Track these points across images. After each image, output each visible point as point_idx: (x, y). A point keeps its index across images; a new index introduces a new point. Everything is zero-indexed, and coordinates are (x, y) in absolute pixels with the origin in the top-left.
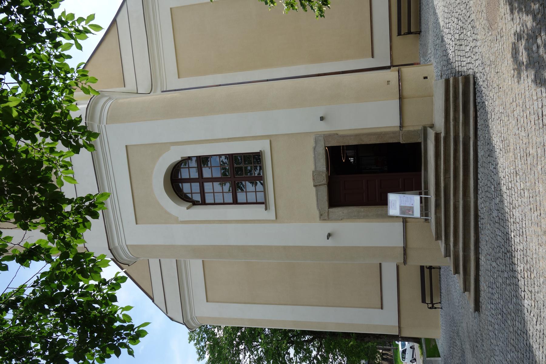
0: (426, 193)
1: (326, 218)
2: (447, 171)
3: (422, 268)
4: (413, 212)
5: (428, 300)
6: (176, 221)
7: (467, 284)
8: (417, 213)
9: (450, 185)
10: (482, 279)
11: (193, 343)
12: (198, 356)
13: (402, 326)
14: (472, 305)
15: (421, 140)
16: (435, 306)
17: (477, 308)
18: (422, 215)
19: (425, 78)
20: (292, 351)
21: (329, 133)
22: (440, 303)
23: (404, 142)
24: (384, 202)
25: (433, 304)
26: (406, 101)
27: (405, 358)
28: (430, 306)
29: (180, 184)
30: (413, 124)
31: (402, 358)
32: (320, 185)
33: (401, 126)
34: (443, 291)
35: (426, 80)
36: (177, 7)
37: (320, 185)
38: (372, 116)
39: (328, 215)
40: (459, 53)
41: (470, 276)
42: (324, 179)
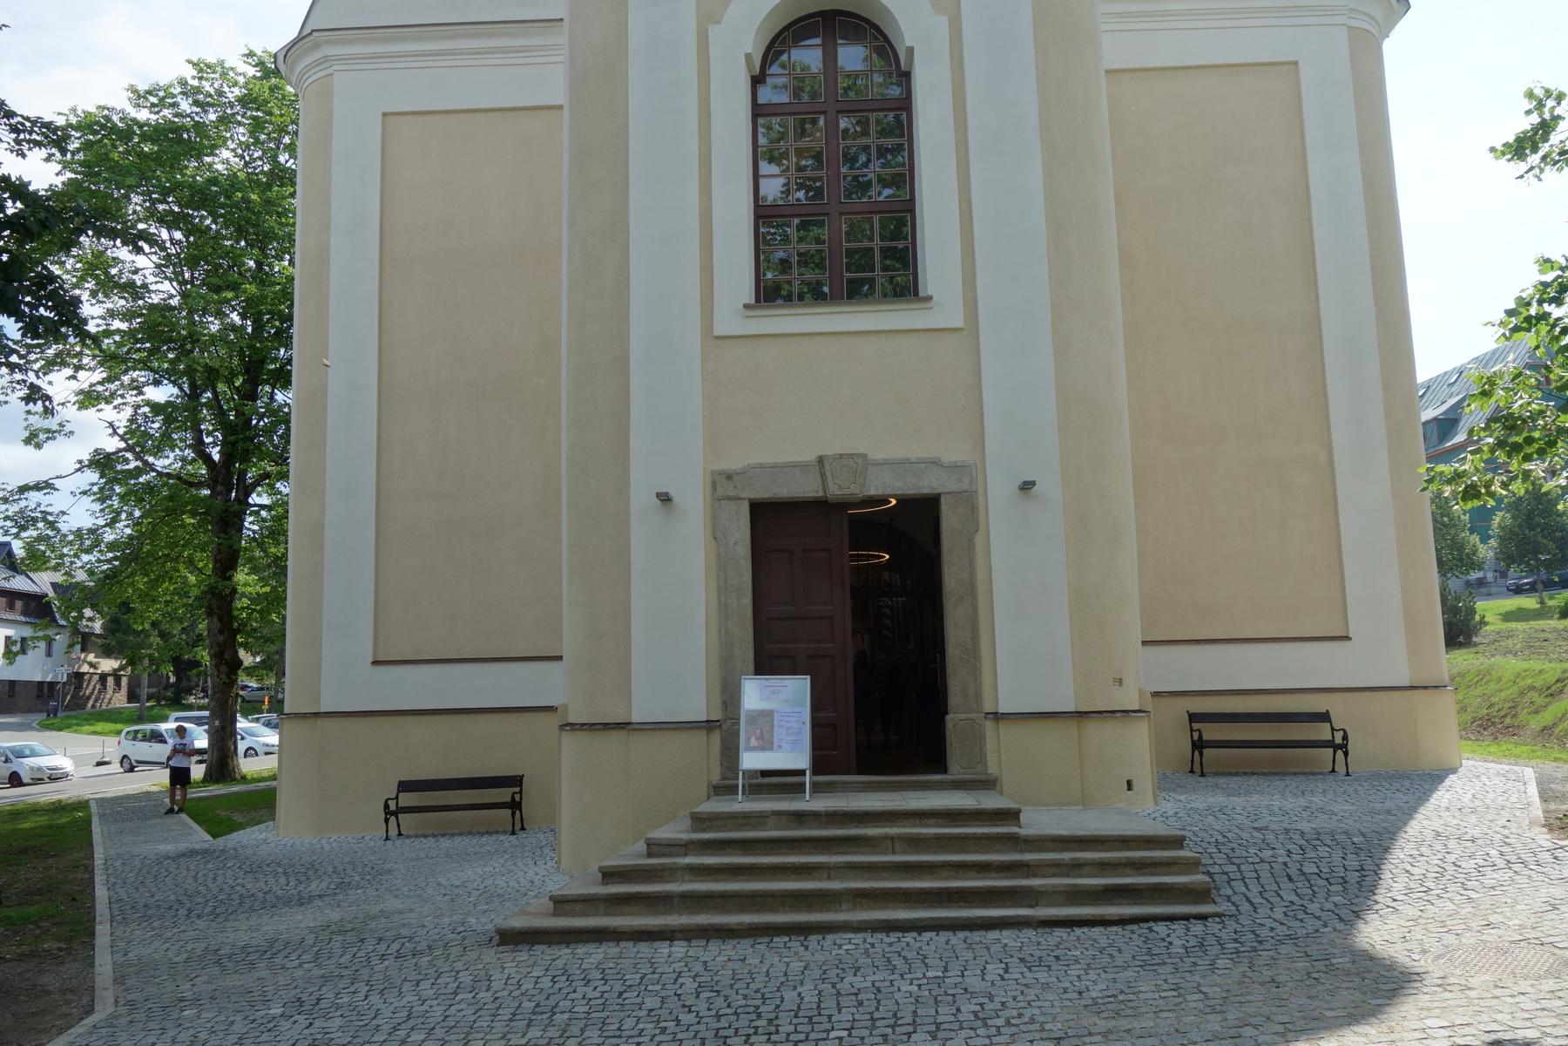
0: (817, 788)
1: (720, 491)
2: (915, 843)
3: (516, 781)
4: (754, 749)
5: (407, 799)
6: (707, 18)
7: (578, 907)
8: (751, 760)
9: (977, 852)
10: (611, 949)
11: (189, 73)
12: (142, 87)
13: (320, 721)
14: (518, 923)
15: (956, 770)
16: (393, 819)
17: (511, 938)
18: (751, 774)
19: (1130, 785)
20: (162, 393)
21: (981, 507)
22: (400, 834)
23: (949, 725)
24: (767, 663)
25: (395, 814)
26: (1071, 728)
27: (135, 739)
28: (393, 806)
29: (818, 41)
30: (1004, 752)
31: (136, 732)
32: (823, 475)
33: (997, 717)
34: (445, 843)
35: (1135, 786)
36: (1297, 83)
37: (823, 475)
38: (1022, 636)
39: (730, 498)
40: (1265, 875)
41: (606, 914)
42: (841, 487)
